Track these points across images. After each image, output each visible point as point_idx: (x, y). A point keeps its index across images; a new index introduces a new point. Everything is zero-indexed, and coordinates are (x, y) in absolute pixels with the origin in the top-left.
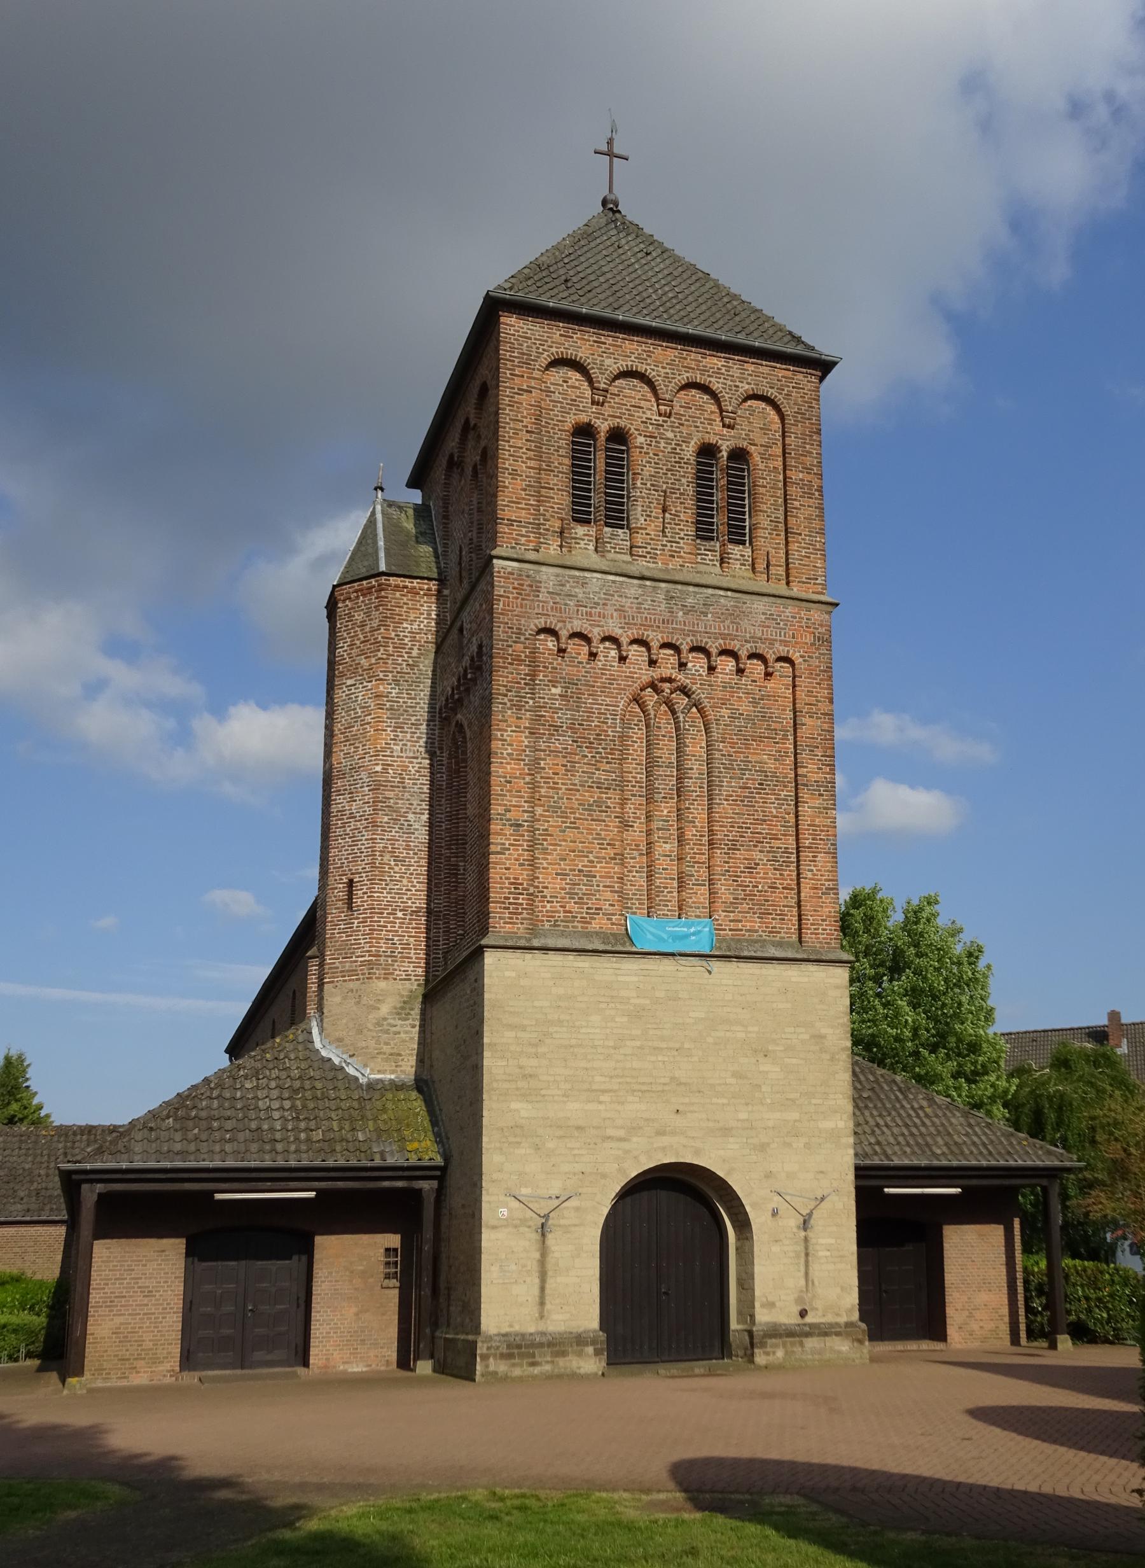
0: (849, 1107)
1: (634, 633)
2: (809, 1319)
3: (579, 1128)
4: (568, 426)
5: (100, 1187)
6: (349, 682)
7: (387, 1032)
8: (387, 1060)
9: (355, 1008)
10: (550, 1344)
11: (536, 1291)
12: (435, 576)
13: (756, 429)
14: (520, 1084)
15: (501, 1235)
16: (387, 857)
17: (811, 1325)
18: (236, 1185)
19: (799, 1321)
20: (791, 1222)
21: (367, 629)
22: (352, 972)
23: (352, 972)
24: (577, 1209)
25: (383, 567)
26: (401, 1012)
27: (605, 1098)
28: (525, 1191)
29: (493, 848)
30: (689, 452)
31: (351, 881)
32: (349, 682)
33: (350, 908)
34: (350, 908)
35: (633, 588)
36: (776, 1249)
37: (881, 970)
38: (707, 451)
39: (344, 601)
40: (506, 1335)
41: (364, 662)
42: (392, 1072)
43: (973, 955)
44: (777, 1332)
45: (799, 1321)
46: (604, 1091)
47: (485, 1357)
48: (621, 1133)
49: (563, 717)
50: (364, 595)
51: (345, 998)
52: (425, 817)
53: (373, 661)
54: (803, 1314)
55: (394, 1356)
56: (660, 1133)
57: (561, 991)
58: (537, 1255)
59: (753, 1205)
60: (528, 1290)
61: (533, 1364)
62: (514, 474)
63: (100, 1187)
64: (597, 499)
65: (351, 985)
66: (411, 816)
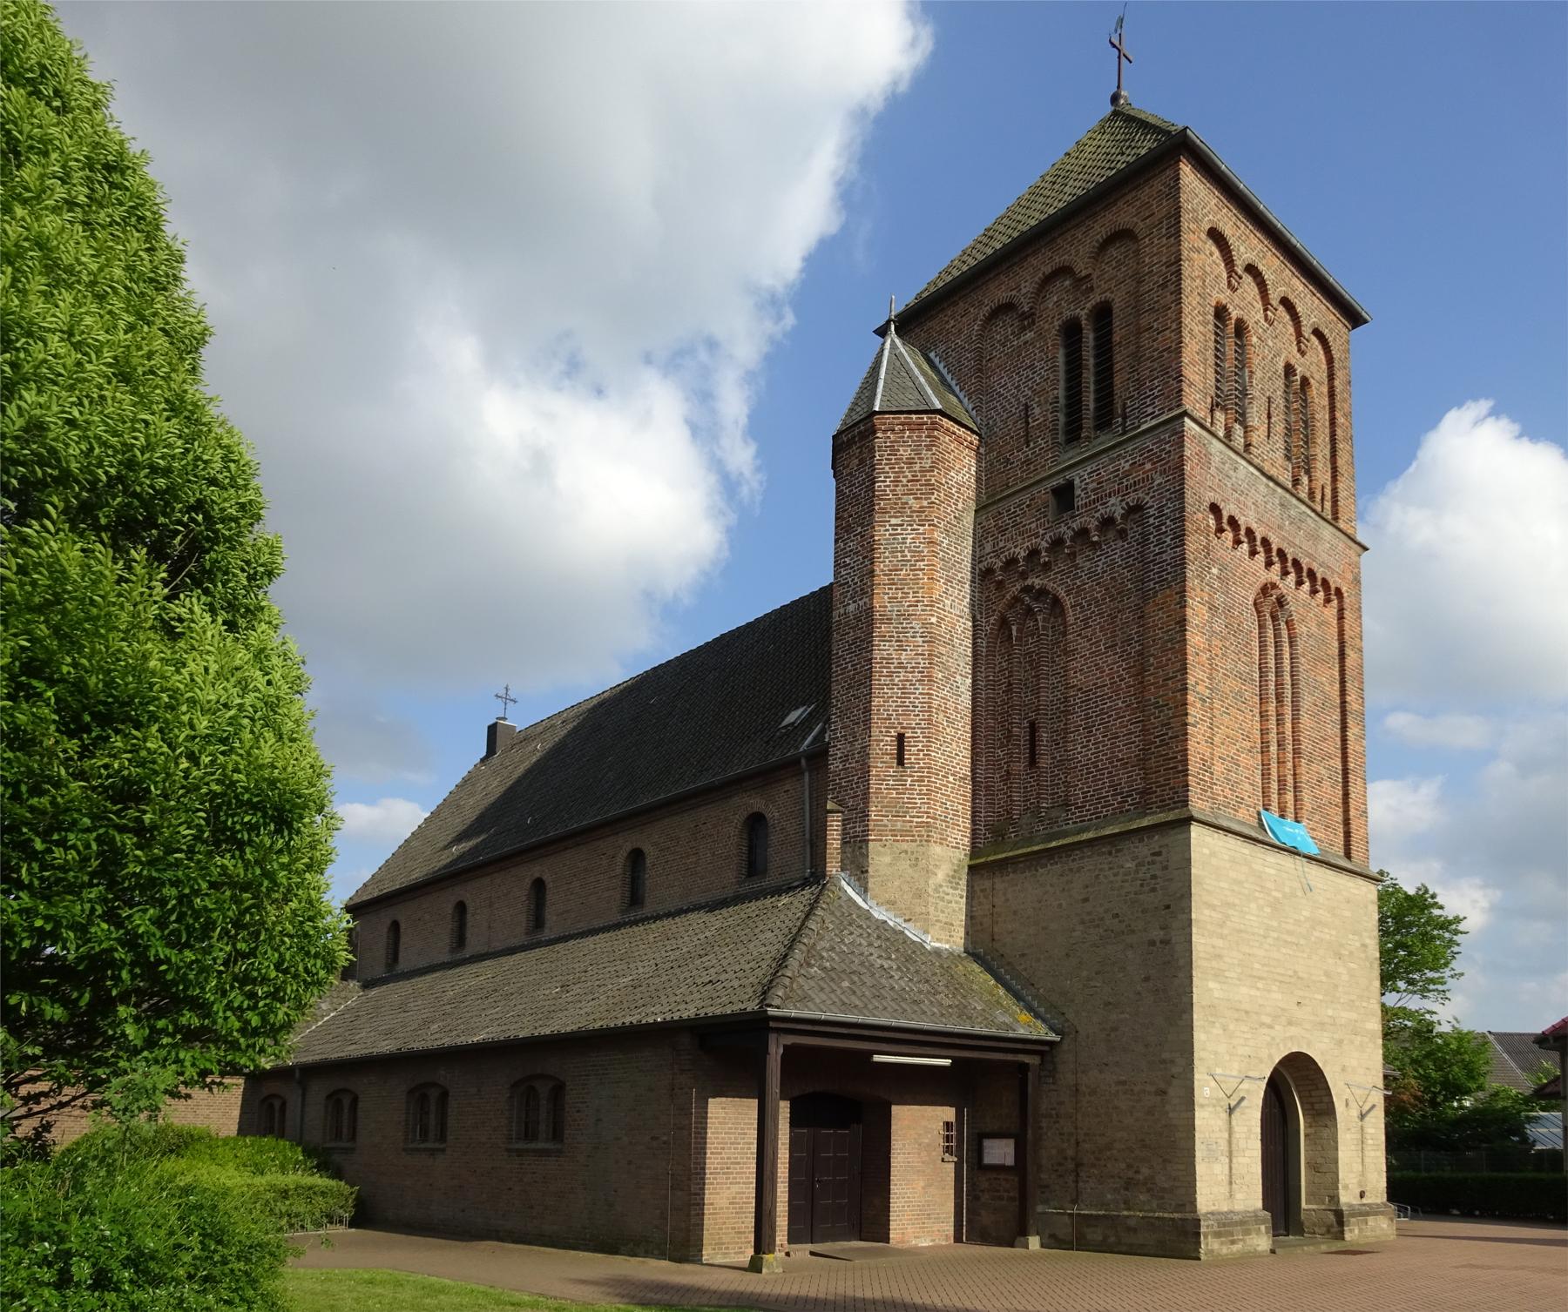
5: (790, 1040)
6: (894, 521)
7: (942, 899)
8: (943, 929)
9: (910, 871)
10: (1242, 1223)
13: (1312, 364)
16: (941, 716)
17: (1368, 1205)
18: (904, 1049)
20: (1355, 1113)
26: (952, 879)
27: (1260, 985)
28: (1219, 1071)
29: (1190, 720)
31: (901, 738)
32: (894, 521)
33: (901, 762)
34: (901, 762)
39: (885, 431)
41: (914, 504)
42: (948, 942)
46: (1260, 978)
48: (1267, 1020)
52: (969, 681)
53: (925, 503)
54: (1362, 1195)
55: (950, 1229)
56: (1290, 1023)
58: (1226, 1135)
61: (1233, 1242)
63: (790, 1040)
64: (1089, 337)
65: (905, 846)
66: (958, 678)
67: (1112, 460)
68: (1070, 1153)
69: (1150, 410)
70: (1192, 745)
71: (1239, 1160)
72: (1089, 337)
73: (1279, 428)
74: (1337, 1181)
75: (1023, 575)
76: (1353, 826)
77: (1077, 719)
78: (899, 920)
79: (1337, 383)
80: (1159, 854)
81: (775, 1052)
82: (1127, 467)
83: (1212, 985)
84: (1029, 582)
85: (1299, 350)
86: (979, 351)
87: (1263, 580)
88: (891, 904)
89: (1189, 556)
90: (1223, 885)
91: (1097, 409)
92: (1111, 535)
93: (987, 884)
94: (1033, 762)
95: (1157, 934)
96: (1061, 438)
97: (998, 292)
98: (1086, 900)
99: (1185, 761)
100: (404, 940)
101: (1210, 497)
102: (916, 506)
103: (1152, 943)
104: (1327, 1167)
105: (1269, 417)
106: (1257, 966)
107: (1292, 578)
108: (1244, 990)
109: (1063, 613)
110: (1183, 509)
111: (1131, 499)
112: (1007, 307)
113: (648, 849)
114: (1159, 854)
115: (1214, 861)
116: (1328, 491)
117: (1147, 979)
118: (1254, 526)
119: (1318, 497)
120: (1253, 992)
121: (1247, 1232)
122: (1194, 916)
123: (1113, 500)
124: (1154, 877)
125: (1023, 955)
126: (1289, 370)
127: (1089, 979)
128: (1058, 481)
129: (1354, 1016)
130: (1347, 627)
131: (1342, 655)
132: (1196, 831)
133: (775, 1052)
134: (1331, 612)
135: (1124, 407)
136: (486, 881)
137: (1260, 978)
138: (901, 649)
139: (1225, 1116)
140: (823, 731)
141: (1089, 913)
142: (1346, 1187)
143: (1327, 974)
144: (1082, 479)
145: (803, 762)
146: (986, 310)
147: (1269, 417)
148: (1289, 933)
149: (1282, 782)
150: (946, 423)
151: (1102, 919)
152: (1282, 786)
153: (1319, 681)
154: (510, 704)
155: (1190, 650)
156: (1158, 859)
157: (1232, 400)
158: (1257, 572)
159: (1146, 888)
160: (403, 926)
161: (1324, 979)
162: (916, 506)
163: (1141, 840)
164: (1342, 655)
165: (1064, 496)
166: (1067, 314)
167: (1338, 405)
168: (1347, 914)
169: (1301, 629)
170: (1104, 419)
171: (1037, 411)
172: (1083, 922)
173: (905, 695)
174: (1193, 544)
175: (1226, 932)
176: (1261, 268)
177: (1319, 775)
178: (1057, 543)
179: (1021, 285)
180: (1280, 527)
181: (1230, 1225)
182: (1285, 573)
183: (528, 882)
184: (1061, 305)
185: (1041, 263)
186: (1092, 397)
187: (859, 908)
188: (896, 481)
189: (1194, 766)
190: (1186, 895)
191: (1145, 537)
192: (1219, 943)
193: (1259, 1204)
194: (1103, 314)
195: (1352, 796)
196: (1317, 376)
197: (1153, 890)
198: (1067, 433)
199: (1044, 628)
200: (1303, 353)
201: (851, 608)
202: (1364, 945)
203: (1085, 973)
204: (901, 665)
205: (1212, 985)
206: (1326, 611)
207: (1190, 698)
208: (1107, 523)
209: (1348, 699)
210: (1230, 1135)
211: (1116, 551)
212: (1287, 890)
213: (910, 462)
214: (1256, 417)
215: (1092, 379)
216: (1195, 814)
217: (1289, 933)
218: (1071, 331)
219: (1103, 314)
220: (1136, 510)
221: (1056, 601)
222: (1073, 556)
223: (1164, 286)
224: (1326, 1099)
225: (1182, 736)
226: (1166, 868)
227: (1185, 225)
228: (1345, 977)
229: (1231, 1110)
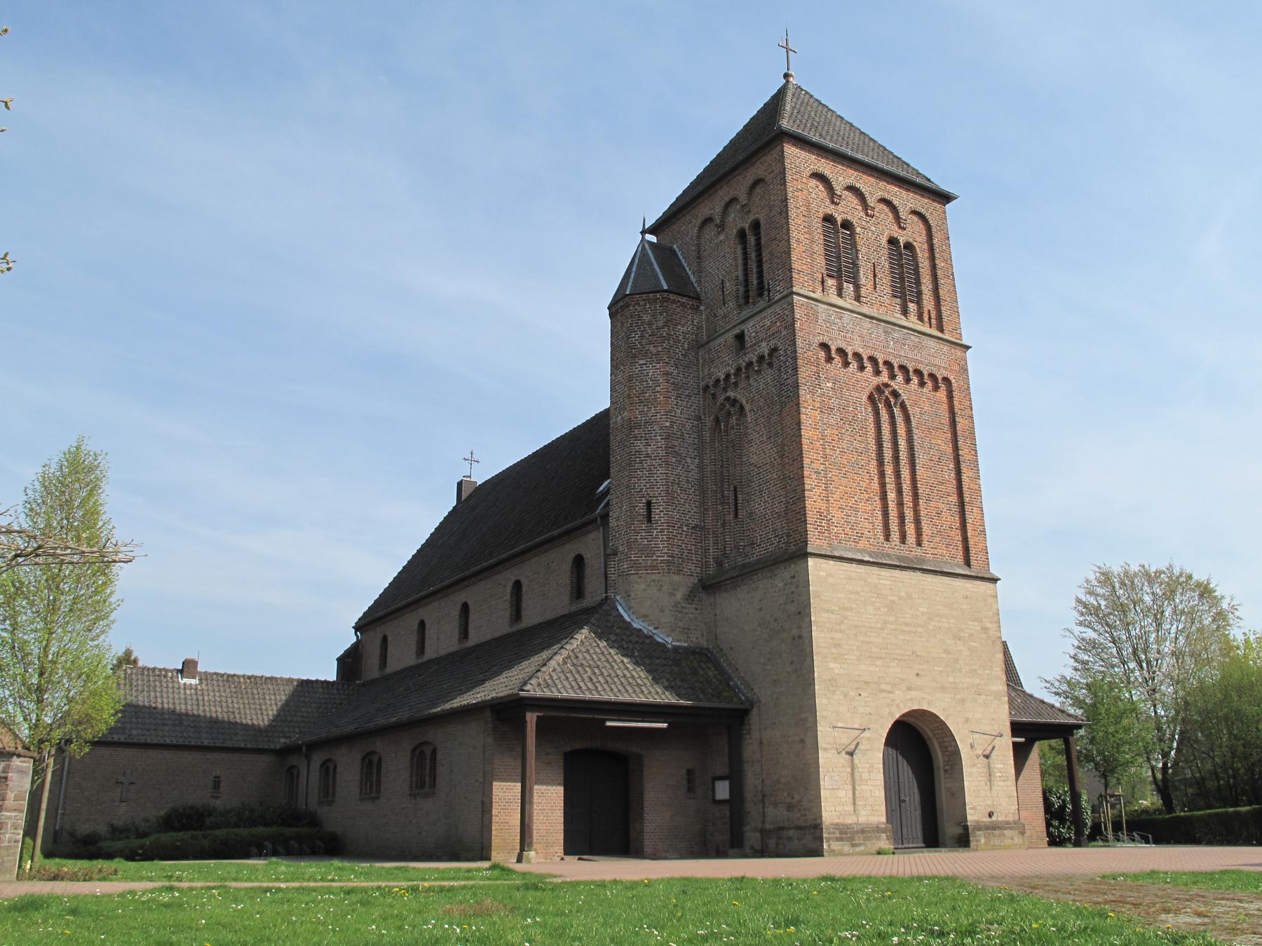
0: (1004, 677)
1: (870, 352)
2: (994, 818)
3: (866, 683)
4: (821, 215)
7: (680, 612)
10: (863, 831)
11: (850, 794)
13: (913, 233)
14: (834, 650)
15: (829, 755)
16: (676, 487)
19: (987, 819)
22: (653, 567)
23: (653, 567)
24: (869, 739)
25: (666, 287)
27: (879, 663)
29: (807, 487)
30: (884, 241)
31: (649, 504)
34: (649, 519)
35: (867, 323)
36: (975, 770)
40: (837, 824)
43: (1106, 578)
44: (979, 827)
45: (987, 819)
47: (828, 840)
48: (888, 688)
49: (834, 402)
54: (990, 815)
56: (909, 689)
57: (851, 588)
59: (962, 740)
60: (845, 794)
62: (798, 241)
64: (751, 240)
65: (653, 577)
66: (689, 460)
70: (809, 504)
72: (751, 240)
75: (725, 389)
76: (971, 542)
79: (935, 241)
80: (793, 577)
81: (531, 718)
85: (900, 227)
88: (645, 617)
89: (801, 381)
90: (839, 595)
94: (736, 515)
95: (795, 632)
98: (761, 610)
100: (390, 649)
102: (654, 351)
103: (794, 638)
105: (875, 276)
106: (874, 649)
107: (900, 378)
108: (862, 667)
110: (796, 352)
111: (772, 344)
112: (708, 220)
113: (524, 581)
114: (793, 577)
115: (830, 580)
116: (933, 315)
118: (861, 351)
119: (926, 319)
120: (872, 668)
126: (892, 241)
128: (737, 331)
129: (978, 681)
131: (953, 424)
132: (811, 561)
133: (531, 718)
134: (942, 394)
136: (435, 604)
144: (749, 328)
146: (699, 222)
147: (875, 276)
148: (906, 624)
150: (672, 297)
153: (932, 446)
154: (475, 464)
155: (804, 441)
157: (842, 267)
158: (869, 380)
160: (390, 639)
161: (944, 655)
162: (654, 351)
164: (953, 424)
166: (739, 225)
167: (937, 256)
174: (804, 373)
175: (843, 627)
176: (858, 185)
177: (938, 510)
178: (739, 369)
179: (711, 207)
181: (847, 833)
183: (459, 606)
184: (736, 221)
185: (723, 195)
187: (624, 621)
188: (642, 337)
189: (811, 517)
192: (839, 635)
193: (883, 819)
194: (756, 226)
196: (918, 239)
204: (648, 456)
206: (938, 394)
210: (853, 770)
211: (769, 375)
212: (903, 594)
217: (906, 624)
218: (742, 235)
219: (756, 226)
220: (774, 350)
221: (742, 407)
223: (780, 214)
225: (802, 498)
227: (789, 178)
229: (851, 754)
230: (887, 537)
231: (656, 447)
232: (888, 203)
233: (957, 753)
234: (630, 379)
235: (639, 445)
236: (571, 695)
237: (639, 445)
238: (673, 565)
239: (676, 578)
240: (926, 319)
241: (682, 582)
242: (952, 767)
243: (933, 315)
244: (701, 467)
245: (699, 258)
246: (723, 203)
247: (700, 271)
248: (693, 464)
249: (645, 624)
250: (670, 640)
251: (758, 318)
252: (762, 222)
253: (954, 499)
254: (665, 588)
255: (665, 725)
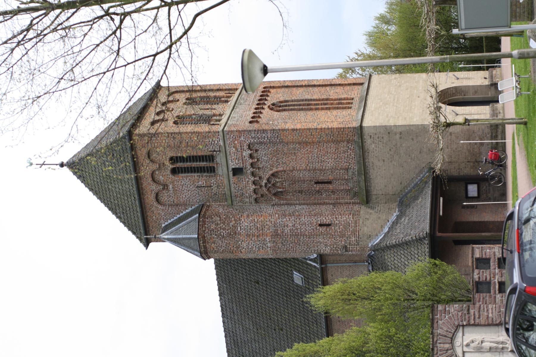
6: (239, 229)
7: (380, 211)
9: (370, 221)
12: (167, 8)
21: (219, 222)
22: (356, 222)
23: (356, 222)
25: (197, 215)
29: (327, 127)
31: (321, 225)
32: (239, 229)
34: (329, 225)
37: (356, 339)
38: (174, 171)
50: (205, 224)
51: (365, 225)
53: (233, 219)
54: (485, 78)
64: (180, 165)
65: (361, 223)
67: (230, 154)
68: (472, 164)
69: (216, 142)
71: (473, 112)
72: (180, 165)
73: (209, 106)
74: (481, 86)
77: (318, 166)
78: (388, 224)
80: (371, 136)
81: (439, 234)
82: (234, 149)
83: (415, 120)
84: (263, 184)
86: (169, 205)
87: (268, 110)
88: (382, 227)
91: (206, 161)
92: (255, 155)
93: (374, 197)
95: (398, 136)
96: (212, 174)
97: (150, 198)
98: (384, 161)
99: (340, 128)
101: (247, 124)
102: (234, 222)
103: (401, 138)
104: (476, 89)
109: (277, 172)
111: (246, 147)
114: (371, 136)
116: (227, 92)
117: (413, 139)
118: (252, 112)
121: (497, 109)
122: (393, 125)
123: (244, 154)
124: (378, 138)
125: (401, 184)
127: (412, 159)
128: (231, 174)
130: (277, 85)
133: (439, 234)
135: (211, 151)
137: (411, 107)
138: (287, 226)
139: (458, 116)
140: (311, 260)
141: (388, 159)
142: (483, 83)
143: (407, 89)
144: (233, 165)
145: (323, 266)
146: (155, 204)
148: (394, 100)
149: (339, 104)
150: (202, 213)
151: (391, 155)
152: (343, 104)
156: (372, 136)
158: (266, 111)
159: (382, 140)
161: (409, 90)
162: (234, 222)
163: (365, 142)
165: (237, 172)
166: (169, 172)
168: (384, 84)
169: (282, 99)
170: (210, 158)
171: (200, 183)
172: (391, 161)
173: (305, 224)
175: (396, 117)
178: (253, 174)
180: (249, 105)
182: (265, 104)
184: (165, 176)
186: (201, 163)
188: (224, 229)
190: (385, 127)
191: (261, 143)
193: (488, 107)
195: (340, 83)
196: (184, 96)
197: (383, 138)
198: (211, 172)
199: (282, 178)
200: (178, 100)
201: (269, 245)
202: (395, 78)
203: (409, 160)
204: (294, 226)
205: (415, 120)
207: (319, 127)
208: (251, 156)
209: (304, 84)
213: (217, 224)
214: (208, 112)
215: (195, 163)
216: (359, 124)
217: (394, 100)
222: (259, 168)
224: (451, 89)
226: (376, 134)
228: (407, 84)
229: (457, 115)
230: (351, 108)
231: (289, 222)
232: (153, 123)
233: (456, 88)
234: (248, 235)
235: (287, 230)
236: (428, 221)
237: (287, 230)
238: (356, 214)
239: (361, 212)
240: (229, 95)
241: (363, 210)
242: (463, 91)
243: (227, 92)
244: (300, 204)
245: (177, 205)
246: (152, 183)
247: (185, 205)
248: (298, 207)
249: (386, 227)
250: (395, 214)
251: (229, 157)
252: (173, 154)
253: (328, 88)
254: (367, 217)
255: (441, 199)
